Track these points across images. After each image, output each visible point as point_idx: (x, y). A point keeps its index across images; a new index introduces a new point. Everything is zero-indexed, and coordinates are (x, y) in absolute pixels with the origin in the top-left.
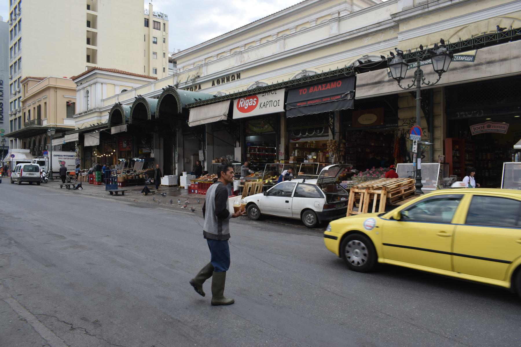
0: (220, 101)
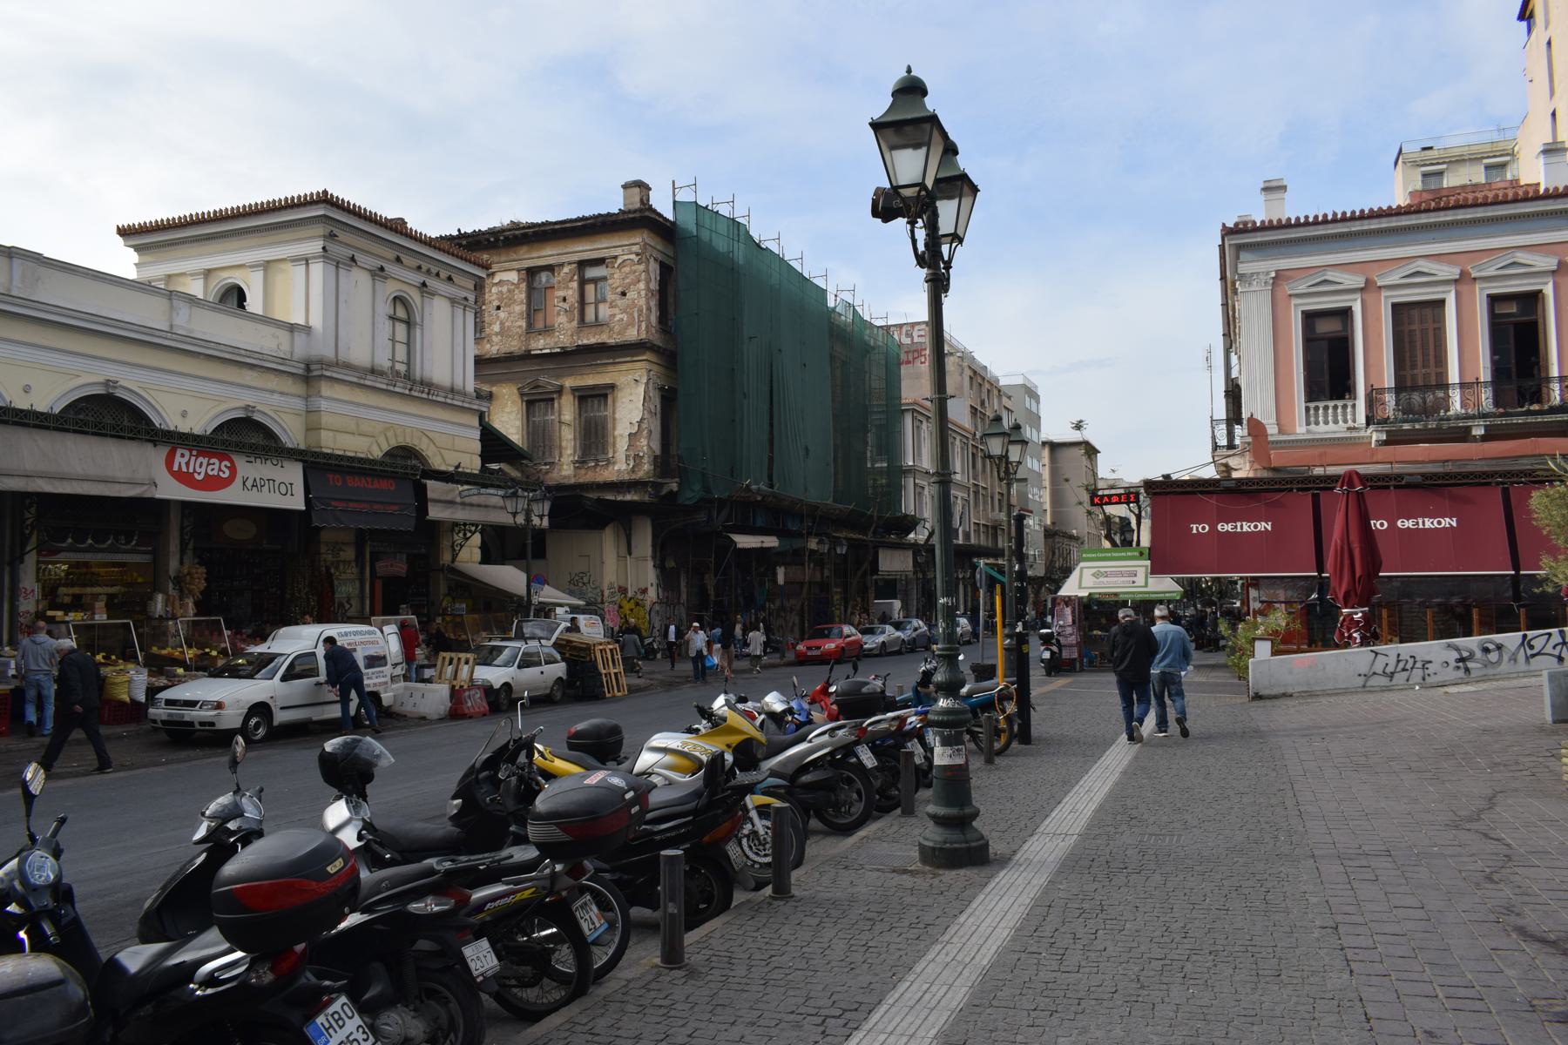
0: (47, 428)
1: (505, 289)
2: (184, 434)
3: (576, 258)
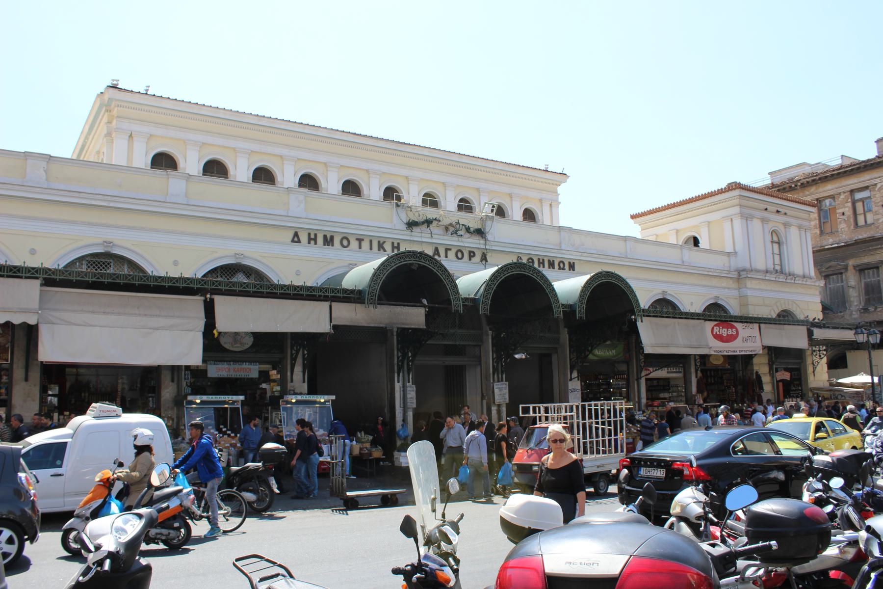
2: (693, 313)
3: (849, 188)
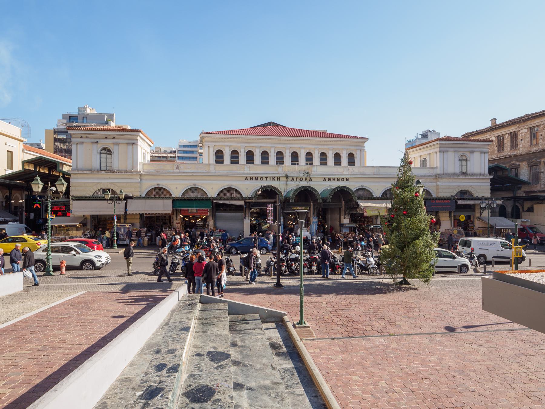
1: (523, 134)
